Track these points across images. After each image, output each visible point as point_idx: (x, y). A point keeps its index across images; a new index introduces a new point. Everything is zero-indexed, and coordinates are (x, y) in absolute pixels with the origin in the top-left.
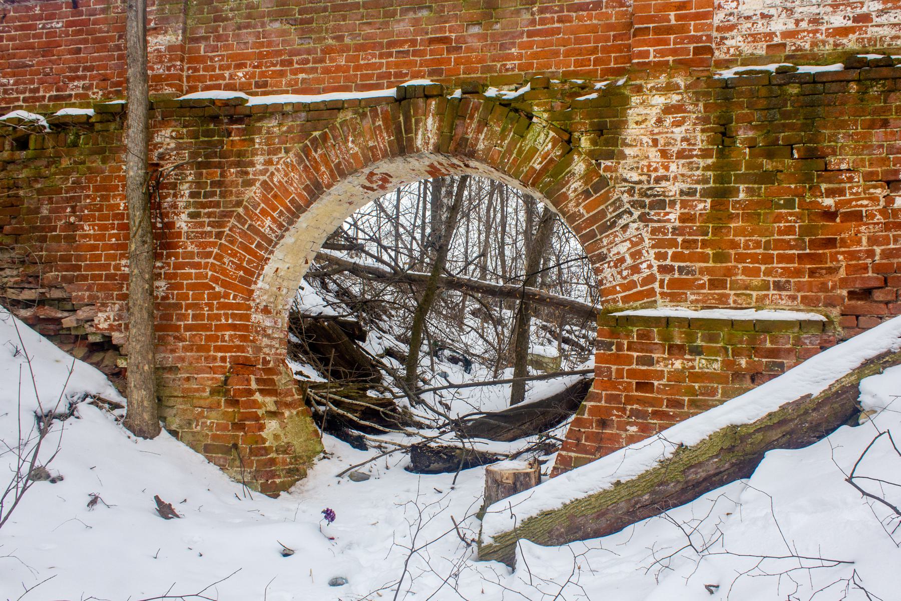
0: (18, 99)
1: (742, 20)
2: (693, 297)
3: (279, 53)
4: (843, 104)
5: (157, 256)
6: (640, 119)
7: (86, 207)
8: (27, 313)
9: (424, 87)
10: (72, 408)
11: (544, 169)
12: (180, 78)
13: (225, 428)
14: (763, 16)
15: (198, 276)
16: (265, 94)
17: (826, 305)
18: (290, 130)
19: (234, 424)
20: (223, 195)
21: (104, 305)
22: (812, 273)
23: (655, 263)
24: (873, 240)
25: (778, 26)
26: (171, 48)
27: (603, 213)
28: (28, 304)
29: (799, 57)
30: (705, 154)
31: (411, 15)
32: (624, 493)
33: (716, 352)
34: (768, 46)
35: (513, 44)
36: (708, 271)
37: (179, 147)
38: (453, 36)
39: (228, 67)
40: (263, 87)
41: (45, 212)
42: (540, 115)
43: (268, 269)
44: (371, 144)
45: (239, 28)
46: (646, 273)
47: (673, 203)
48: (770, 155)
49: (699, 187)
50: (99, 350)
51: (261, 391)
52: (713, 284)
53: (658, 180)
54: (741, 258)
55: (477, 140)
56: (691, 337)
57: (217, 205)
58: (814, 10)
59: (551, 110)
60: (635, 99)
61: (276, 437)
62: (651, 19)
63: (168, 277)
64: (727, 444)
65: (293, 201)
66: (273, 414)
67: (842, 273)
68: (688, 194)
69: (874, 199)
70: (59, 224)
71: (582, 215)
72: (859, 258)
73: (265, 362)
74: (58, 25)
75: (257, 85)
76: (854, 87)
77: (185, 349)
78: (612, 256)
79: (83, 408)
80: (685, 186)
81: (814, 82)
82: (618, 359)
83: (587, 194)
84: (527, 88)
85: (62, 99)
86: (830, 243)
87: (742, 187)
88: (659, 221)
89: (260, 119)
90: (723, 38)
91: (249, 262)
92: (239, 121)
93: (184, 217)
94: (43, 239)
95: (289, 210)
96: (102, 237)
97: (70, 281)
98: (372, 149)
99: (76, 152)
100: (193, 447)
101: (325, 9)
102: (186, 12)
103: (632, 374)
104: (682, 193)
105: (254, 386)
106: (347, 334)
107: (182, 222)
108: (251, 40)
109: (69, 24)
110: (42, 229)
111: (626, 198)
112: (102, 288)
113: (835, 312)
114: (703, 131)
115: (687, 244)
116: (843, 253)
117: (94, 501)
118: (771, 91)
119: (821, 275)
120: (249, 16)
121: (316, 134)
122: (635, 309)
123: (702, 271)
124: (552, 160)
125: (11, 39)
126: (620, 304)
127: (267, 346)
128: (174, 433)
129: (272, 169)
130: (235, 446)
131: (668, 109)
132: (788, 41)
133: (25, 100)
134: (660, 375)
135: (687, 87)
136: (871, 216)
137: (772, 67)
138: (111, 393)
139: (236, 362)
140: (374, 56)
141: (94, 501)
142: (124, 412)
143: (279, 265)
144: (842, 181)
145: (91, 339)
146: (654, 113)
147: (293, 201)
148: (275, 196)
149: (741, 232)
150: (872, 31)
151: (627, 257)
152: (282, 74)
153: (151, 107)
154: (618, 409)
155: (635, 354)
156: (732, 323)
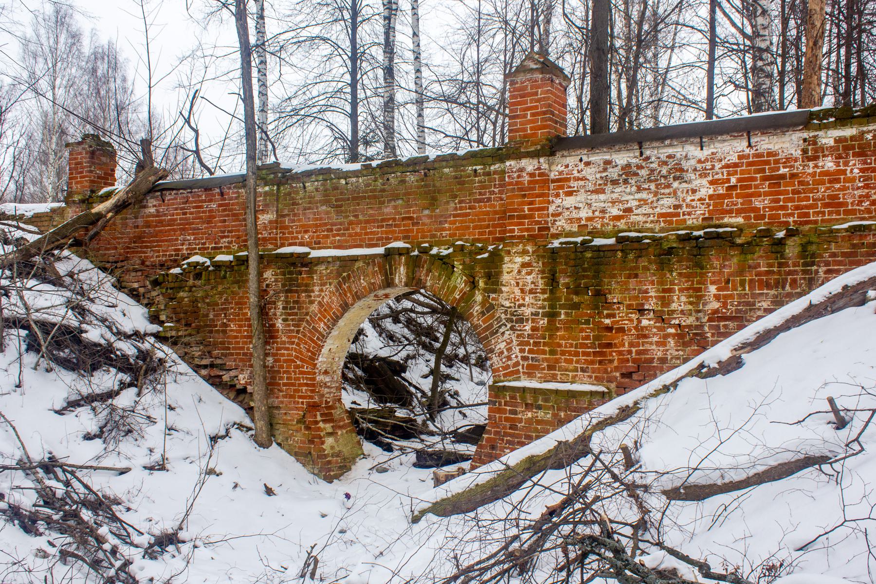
0: (195, 249)
1: (565, 210)
2: (539, 375)
3: (326, 224)
4: (614, 264)
5: (267, 343)
6: (509, 270)
7: (231, 314)
8: (204, 372)
9: (399, 248)
10: (227, 431)
11: (462, 298)
12: (276, 239)
13: (304, 443)
14: (576, 208)
15: (289, 355)
16: (319, 248)
17: (608, 382)
18: (331, 272)
19: (309, 441)
20: (299, 309)
21: (242, 370)
22: (600, 362)
23: (519, 355)
24: (631, 345)
25: (584, 214)
26: (270, 222)
27: (491, 325)
28: (205, 367)
29: (595, 234)
30: (543, 292)
31: (393, 203)
32: (479, 490)
33: (548, 408)
34: (579, 226)
35: (446, 221)
36: (547, 360)
37: (276, 281)
38: (415, 215)
39: (300, 232)
40: (317, 244)
41: (211, 316)
42: (458, 267)
43: (325, 351)
44: (372, 281)
45: (305, 210)
46: (515, 360)
47: (527, 320)
48: (577, 293)
49: (541, 311)
50: (239, 394)
51: (324, 421)
52: (550, 368)
53: (520, 306)
54: (563, 353)
55: (426, 280)
56: (536, 400)
57: (296, 314)
58: (602, 205)
59: (464, 264)
60: (506, 259)
61: (332, 448)
62: (515, 210)
63: (274, 355)
64: (527, 466)
65: (334, 313)
66: (330, 434)
67: (616, 363)
68: (535, 315)
69: (631, 320)
70: (219, 323)
71: (481, 326)
72: (624, 355)
73: (327, 402)
74: (214, 206)
75: (316, 243)
76: (619, 254)
77: (285, 396)
78: (497, 351)
79: (234, 432)
80: (533, 310)
81: (599, 251)
82: (500, 411)
83: (483, 313)
84: (451, 250)
85: (217, 250)
86: (609, 345)
87: (563, 311)
88: (520, 330)
89: (316, 265)
90: (555, 221)
91: (314, 348)
92: (306, 265)
93: (280, 321)
94: (211, 332)
95: (332, 318)
96: (240, 332)
97: (225, 355)
98: (373, 284)
99: (225, 281)
100: (289, 453)
101: (348, 199)
102: (277, 200)
103: (507, 419)
104: (532, 314)
105: (319, 418)
106: (391, 370)
107: (279, 324)
108: (311, 216)
109: (220, 205)
110: (210, 326)
111: (503, 316)
112: (241, 360)
113: (613, 386)
114: (542, 278)
115: (536, 344)
116: (615, 352)
117: (236, 486)
118: (576, 256)
119: (605, 364)
120: (310, 203)
121: (345, 274)
122: (510, 381)
123: (544, 360)
124: (465, 293)
125: (191, 213)
126: (502, 378)
127: (328, 393)
128: (279, 444)
129: (323, 294)
130: (310, 453)
131: (524, 265)
132: (589, 223)
133: (199, 249)
134: (520, 420)
135: (534, 252)
136: (630, 330)
137: (579, 239)
138: (247, 422)
139: (308, 404)
140: (374, 227)
141: (236, 486)
142: (253, 432)
143: (331, 347)
144: (614, 309)
145: (238, 387)
146: (516, 267)
147: (334, 313)
148: (325, 310)
149: (562, 338)
150: (633, 218)
151: (505, 351)
152: (327, 237)
153: (261, 257)
154: (500, 439)
155: (508, 408)
156: (557, 392)
